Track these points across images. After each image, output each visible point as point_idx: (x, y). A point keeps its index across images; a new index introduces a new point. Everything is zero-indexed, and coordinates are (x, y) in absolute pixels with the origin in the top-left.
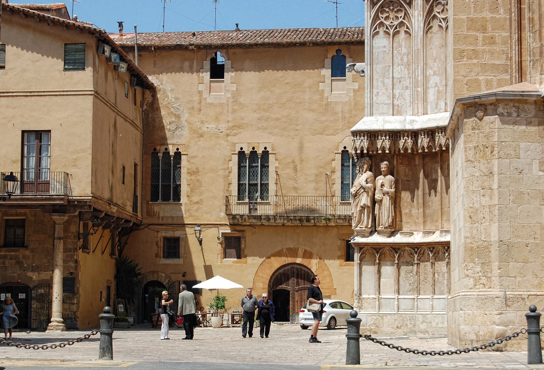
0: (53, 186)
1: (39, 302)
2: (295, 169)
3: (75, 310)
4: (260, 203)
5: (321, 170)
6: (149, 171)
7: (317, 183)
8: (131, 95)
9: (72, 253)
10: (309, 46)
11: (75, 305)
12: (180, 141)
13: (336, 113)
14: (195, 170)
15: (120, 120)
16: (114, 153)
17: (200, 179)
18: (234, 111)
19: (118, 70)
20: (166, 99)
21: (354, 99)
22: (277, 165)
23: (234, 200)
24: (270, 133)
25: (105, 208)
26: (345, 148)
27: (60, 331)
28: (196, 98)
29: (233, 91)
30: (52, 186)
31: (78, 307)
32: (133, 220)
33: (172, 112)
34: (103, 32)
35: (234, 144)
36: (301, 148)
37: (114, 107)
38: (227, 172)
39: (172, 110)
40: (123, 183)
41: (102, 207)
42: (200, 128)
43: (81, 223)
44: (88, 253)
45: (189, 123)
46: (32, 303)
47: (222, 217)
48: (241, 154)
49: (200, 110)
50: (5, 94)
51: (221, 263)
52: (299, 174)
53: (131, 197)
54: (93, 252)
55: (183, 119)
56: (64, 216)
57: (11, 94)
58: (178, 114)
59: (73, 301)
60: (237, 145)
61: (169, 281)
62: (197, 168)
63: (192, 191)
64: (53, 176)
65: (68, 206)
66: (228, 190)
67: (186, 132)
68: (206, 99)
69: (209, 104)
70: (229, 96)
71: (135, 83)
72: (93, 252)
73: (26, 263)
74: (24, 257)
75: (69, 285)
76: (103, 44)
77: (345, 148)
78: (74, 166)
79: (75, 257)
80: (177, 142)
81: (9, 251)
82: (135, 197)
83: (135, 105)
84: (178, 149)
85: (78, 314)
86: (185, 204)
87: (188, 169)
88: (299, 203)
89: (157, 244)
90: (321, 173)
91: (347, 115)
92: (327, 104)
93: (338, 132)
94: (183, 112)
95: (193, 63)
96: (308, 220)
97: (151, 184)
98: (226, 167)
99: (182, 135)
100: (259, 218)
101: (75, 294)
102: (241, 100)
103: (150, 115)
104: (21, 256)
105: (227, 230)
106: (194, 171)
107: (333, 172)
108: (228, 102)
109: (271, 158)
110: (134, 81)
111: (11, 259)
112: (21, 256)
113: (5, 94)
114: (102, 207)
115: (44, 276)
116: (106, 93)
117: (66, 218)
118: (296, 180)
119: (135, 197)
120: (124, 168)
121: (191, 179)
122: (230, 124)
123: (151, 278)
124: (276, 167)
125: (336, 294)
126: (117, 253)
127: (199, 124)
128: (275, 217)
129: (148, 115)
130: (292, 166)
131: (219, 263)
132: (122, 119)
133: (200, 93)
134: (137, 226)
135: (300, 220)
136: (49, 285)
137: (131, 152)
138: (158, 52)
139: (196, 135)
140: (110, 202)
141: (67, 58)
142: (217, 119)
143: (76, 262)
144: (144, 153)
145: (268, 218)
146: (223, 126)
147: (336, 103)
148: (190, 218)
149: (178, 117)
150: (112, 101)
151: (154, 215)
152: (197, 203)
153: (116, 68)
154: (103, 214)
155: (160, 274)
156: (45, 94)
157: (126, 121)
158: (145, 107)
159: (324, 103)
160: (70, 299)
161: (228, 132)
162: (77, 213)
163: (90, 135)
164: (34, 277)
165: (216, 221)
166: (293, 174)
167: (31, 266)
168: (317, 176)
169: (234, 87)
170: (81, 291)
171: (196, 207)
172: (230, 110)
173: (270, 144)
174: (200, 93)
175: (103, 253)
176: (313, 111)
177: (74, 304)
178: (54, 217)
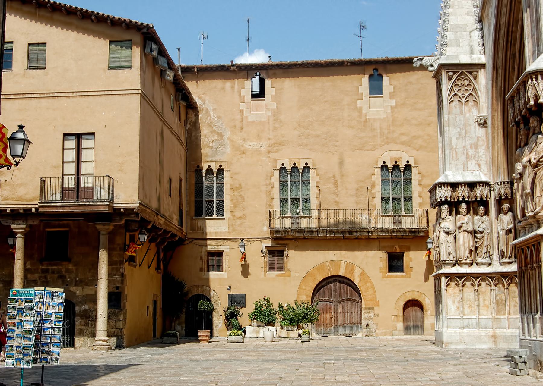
0: (97, 192)
1: (83, 319)
2: (336, 184)
3: (121, 327)
4: (302, 217)
5: (362, 184)
6: (193, 187)
7: (357, 197)
8: (176, 109)
9: (118, 266)
10: (347, 65)
11: (122, 322)
12: (223, 158)
13: (374, 129)
14: (238, 186)
15: (166, 131)
16: (161, 163)
17: (243, 195)
18: (275, 129)
19: (164, 78)
20: (209, 118)
21: (392, 116)
22: (318, 180)
23: (276, 214)
24: (311, 149)
25: (152, 218)
26: (384, 162)
27: (105, 352)
28: (238, 117)
29: (274, 109)
30: (95, 192)
31: (124, 324)
32: (179, 234)
33: (215, 131)
34: (151, 26)
35: (276, 161)
36: (341, 163)
37: (160, 115)
39: (215, 128)
40: (170, 195)
41: (149, 216)
42: (242, 146)
43: (128, 234)
44: (135, 266)
45: (232, 141)
46: (76, 319)
47: (265, 231)
48: (283, 169)
49: (242, 128)
50: (46, 95)
51: (265, 276)
52: (339, 189)
53: (177, 212)
54: (140, 265)
55: (225, 137)
56: (109, 225)
57: (51, 95)
58: (221, 133)
60: (278, 161)
62: (240, 184)
63: (235, 206)
64: (97, 182)
65: (114, 214)
66: (270, 205)
67: (228, 150)
68: (247, 117)
69: (250, 122)
70: (270, 114)
71: (180, 97)
72: (140, 265)
73: (69, 277)
74: (68, 271)
75: (115, 300)
76: (151, 42)
77: (384, 162)
78: (120, 170)
79: (121, 270)
81: (51, 265)
82: (181, 212)
83: (180, 121)
84: (220, 166)
85: (125, 331)
86: (229, 218)
87: (231, 185)
88: (343, 216)
89: (201, 258)
90: (361, 187)
91: (386, 132)
92: (366, 121)
93: (377, 147)
94: (225, 130)
95: (235, 84)
96: (351, 232)
97: (195, 201)
98: (268, 182)
99: (224, 153)
100: (302, 231)
101: (121, 310)
102: (282, 117)
103: (193, 134)
104: (63, 270)
105: (269, 244)
106: (236, 187)
107: (373, 186)
108: (269, 120)
109: (312, 173)
110: (179, 95)
111: (53, 272)
112: (63, 270)
113: (46, 95)
114: (149, 216)
115: (88, 291)
116: (153, 98)
117: (112, 228)
118: (337, 195)
119: (181, 212)
120: (170, 180)
121: (234, 195)
122: (272, 142)
123: (195, 292)
124: (317, 182)
125: (379, 306)
126: (162, 267)
127: (241, 142)
128: (318, 232)
130: (333, 181)
131: (263, 276)
132: (168, 130)
133: (242, 112)
134: (182, 241)
135: (343, 232)
136: (94, 300)
137: (176, 168)
138: (200, 73)
140: (158, 212)
141: (111, 56)
142: (259, 137)
143: (123, 275)
144: (187, 171)
145: (311, 231)
146: (264, 144)
147: (374, 120)
148: (234, 233)
149: (221, 135)
150: (159, 108)
152: (240, 218)
153: (162, 73)
154: (151, 225)
155: (205, 287)
156: (89, 94)
157: (172, 133)
158: (188, 126)
159: (363, 119)
160: (116, 315)
161: (270, 149)
162: (123, 222)
163: (138, 138)
164: (78, 292)
165: (260, 235)
166: (334, 189)
167: (74, 281)
168: (357, 190)
169: (274, 106)
170: (128, 307)
171: (239, 222)
172: (271, 128)
173: (311, 160)
174: (242, 112)
175: (149, 267)
176: (352, 127)
177: (120, 320)
178: (98, 227)
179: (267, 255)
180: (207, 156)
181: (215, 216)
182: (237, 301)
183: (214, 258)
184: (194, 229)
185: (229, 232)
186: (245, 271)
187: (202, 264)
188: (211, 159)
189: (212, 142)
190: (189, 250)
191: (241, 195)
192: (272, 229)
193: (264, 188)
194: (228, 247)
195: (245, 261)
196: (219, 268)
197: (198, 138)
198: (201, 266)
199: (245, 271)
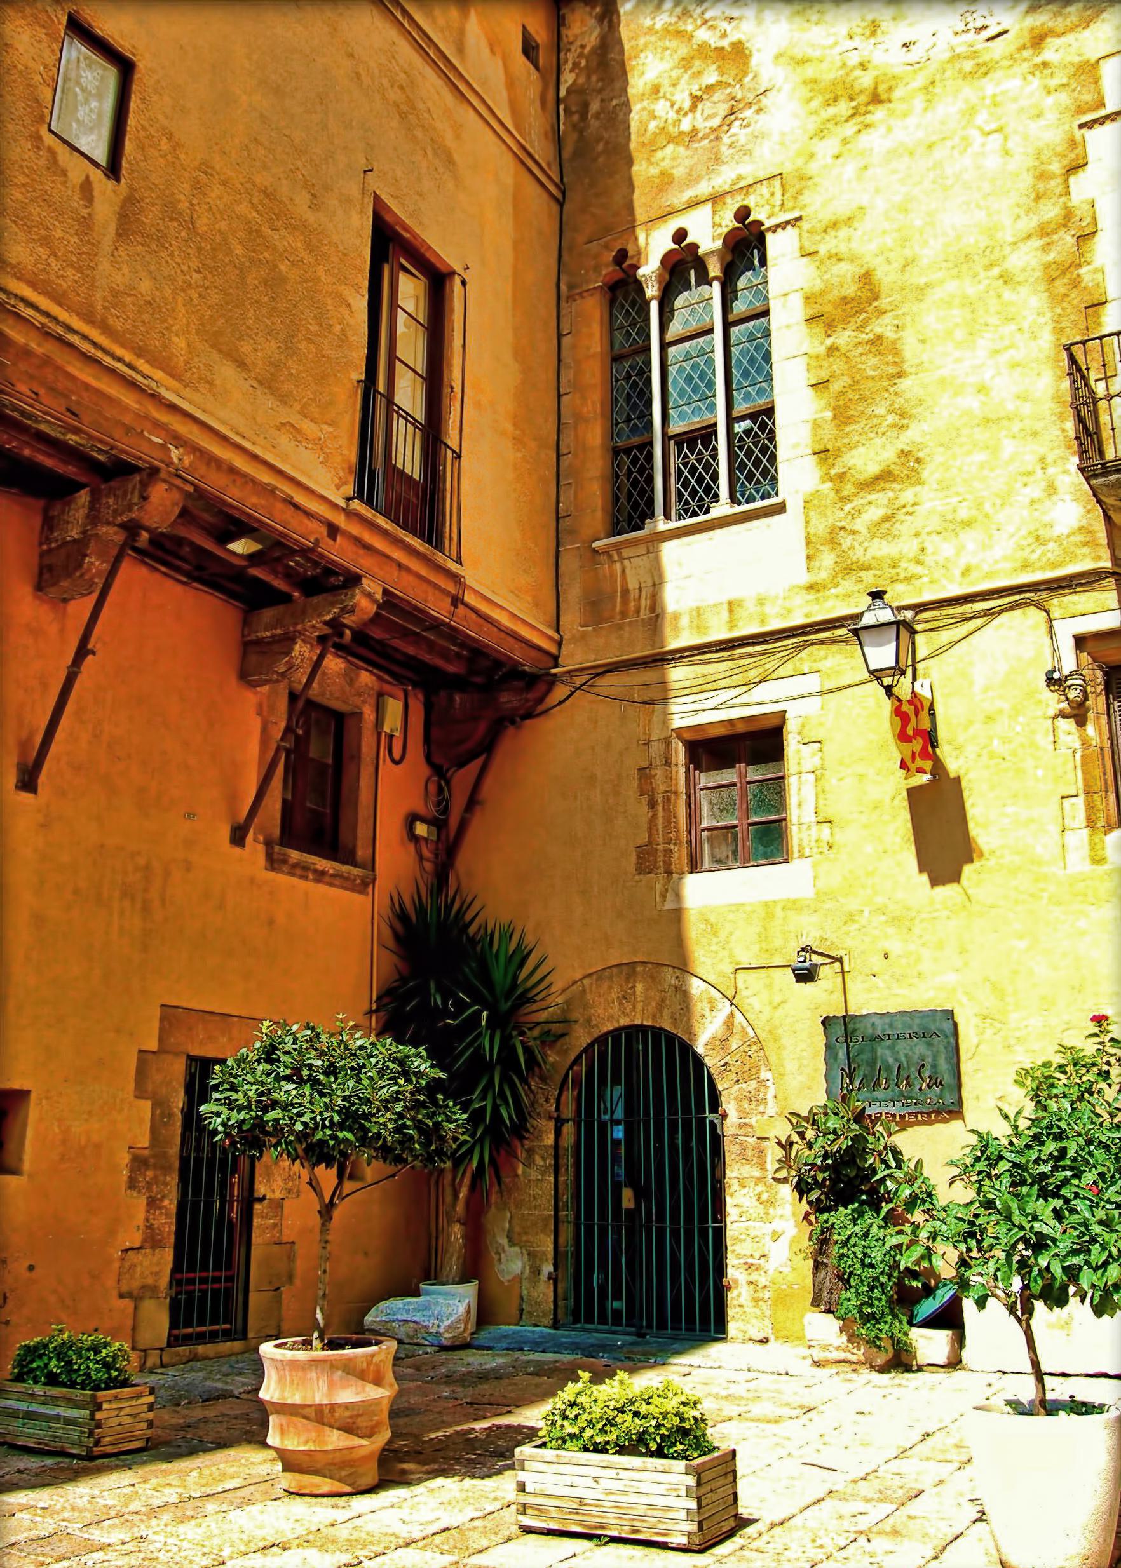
14: (851, 290)
17: (890, 334)
38: (1068, 239)
59: (301, 1128)
61: (729, 1023)
62: (866, 278)
63: (842, 416)
80: (739, 178)
103: (595, 106)
106: (844, 299)
121: (832, 350)
129: (586, 106)
139: (843, 108)
151: (624, 614)
171: (875, 506)
179: (1097, 703)
180: (666, 181)
181: (722, 508)
182: (894, 1062)
183: (728, 776)
184: (600, 608)
185: (811, 587)
186: (941, 833)
187: (653, 820)
188: (689, 194)
189: (693, 108)
190: (566, 742)
191: (877, 340)
192: (1106, 470)
193: (1027, 259)
194: (812, 683)
195: (938, 769)
196: (766, 839)
197: (617, 116)
198: (643, 838)
199: (941, 833)
